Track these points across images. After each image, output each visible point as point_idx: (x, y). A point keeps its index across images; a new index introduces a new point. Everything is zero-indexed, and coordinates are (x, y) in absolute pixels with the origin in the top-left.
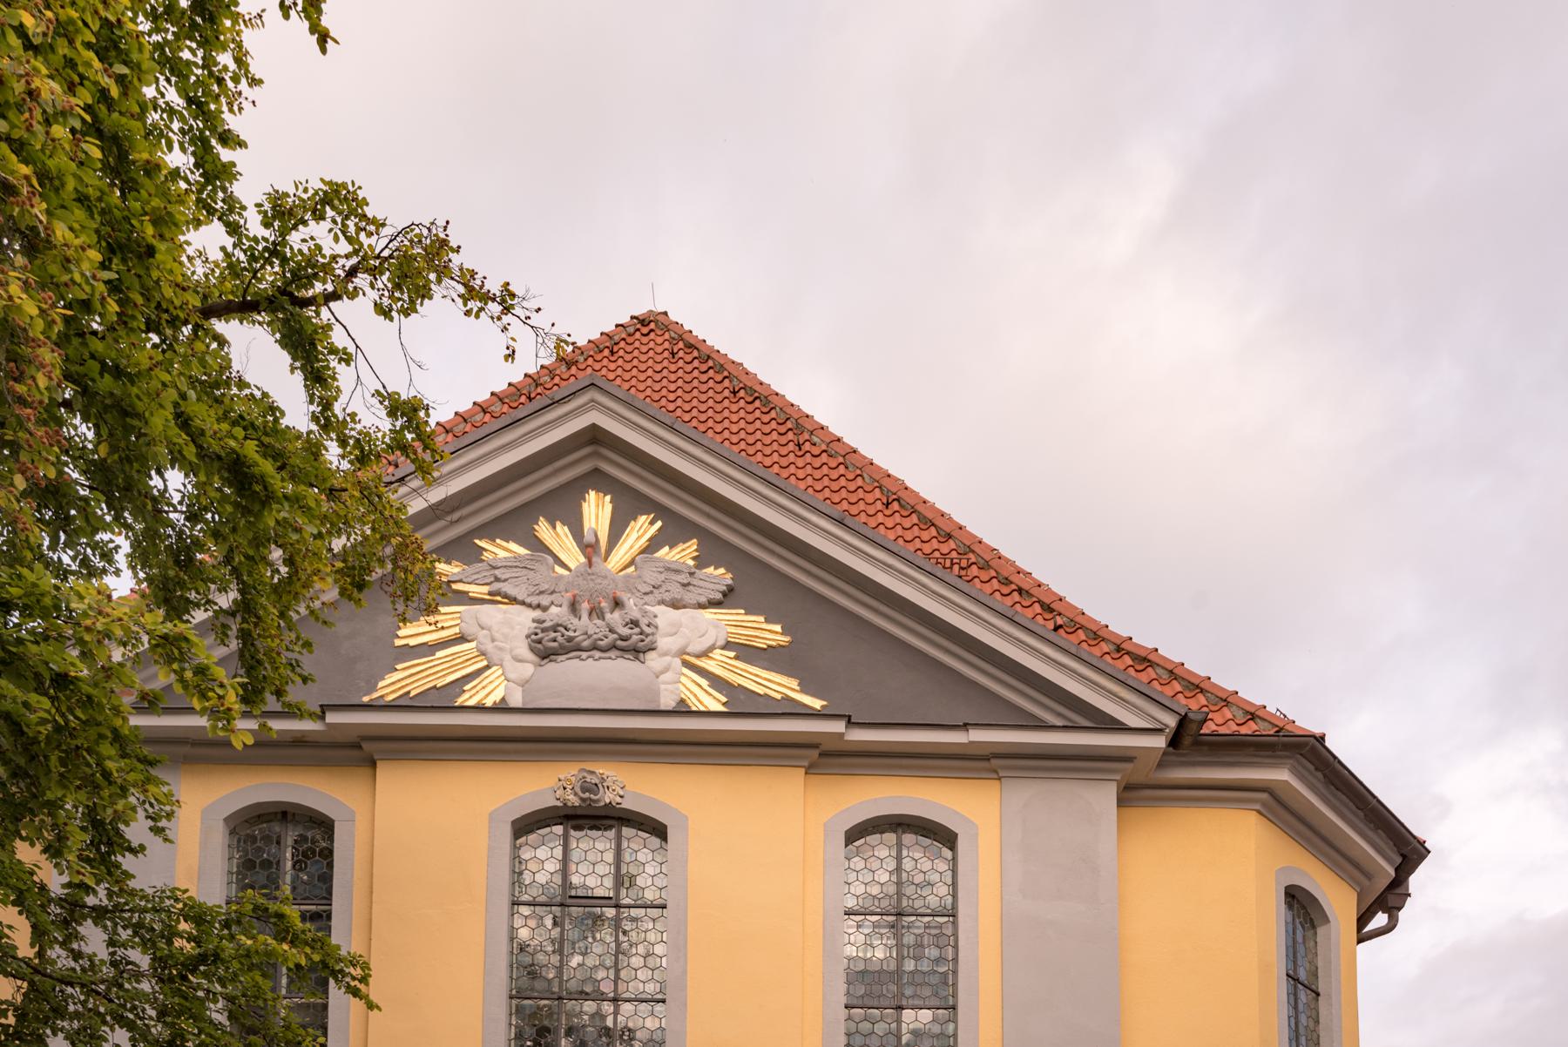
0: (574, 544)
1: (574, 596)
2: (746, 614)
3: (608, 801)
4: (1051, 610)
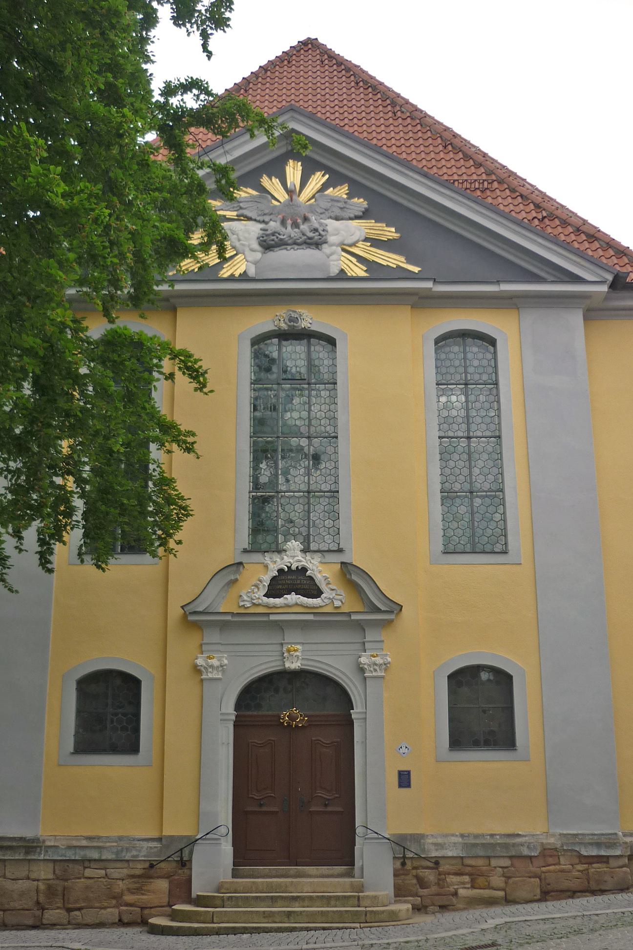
0: (282, 188)
1: (283, 217)
2: (375, 222)
3: (303, 327)
4: (540, 207)
